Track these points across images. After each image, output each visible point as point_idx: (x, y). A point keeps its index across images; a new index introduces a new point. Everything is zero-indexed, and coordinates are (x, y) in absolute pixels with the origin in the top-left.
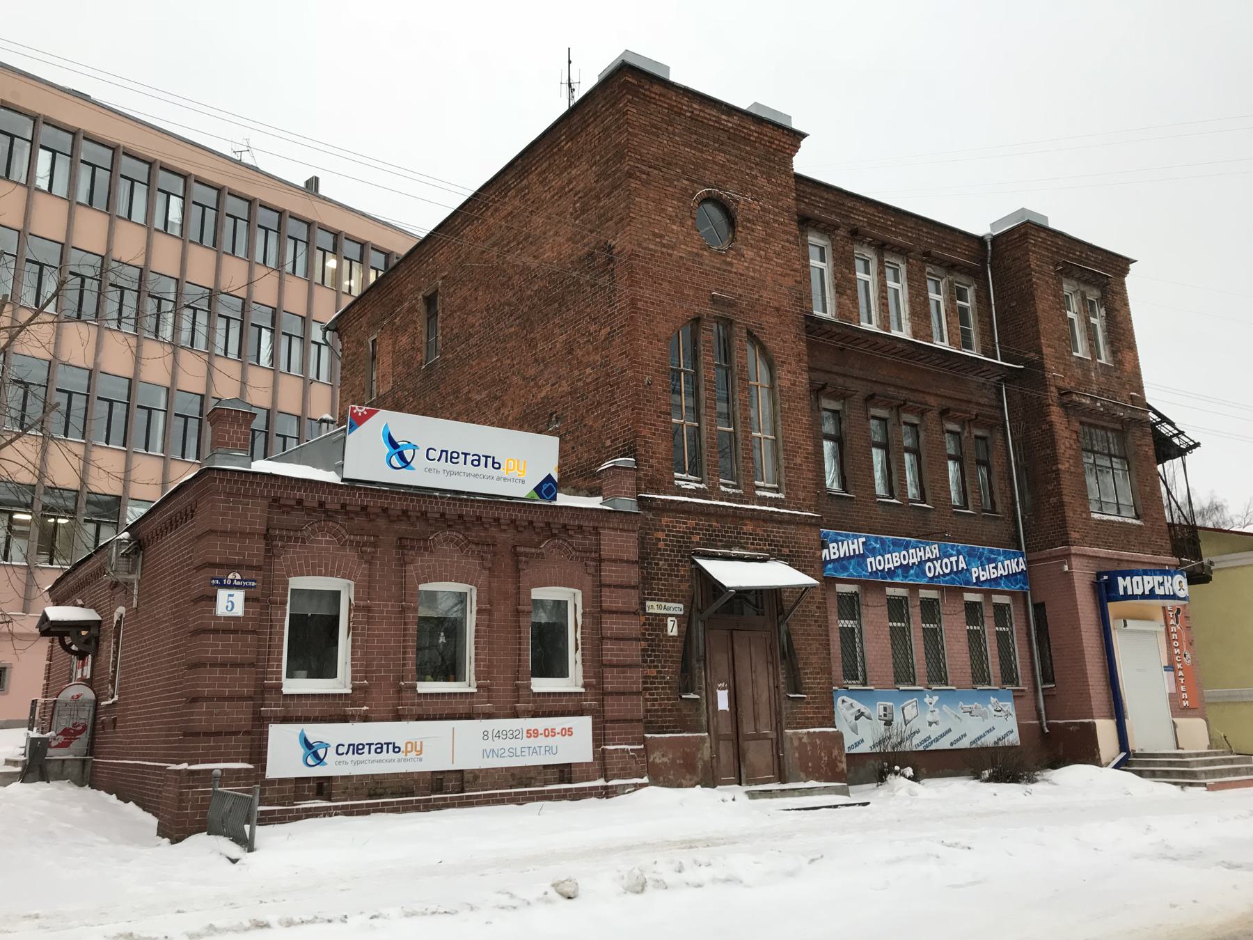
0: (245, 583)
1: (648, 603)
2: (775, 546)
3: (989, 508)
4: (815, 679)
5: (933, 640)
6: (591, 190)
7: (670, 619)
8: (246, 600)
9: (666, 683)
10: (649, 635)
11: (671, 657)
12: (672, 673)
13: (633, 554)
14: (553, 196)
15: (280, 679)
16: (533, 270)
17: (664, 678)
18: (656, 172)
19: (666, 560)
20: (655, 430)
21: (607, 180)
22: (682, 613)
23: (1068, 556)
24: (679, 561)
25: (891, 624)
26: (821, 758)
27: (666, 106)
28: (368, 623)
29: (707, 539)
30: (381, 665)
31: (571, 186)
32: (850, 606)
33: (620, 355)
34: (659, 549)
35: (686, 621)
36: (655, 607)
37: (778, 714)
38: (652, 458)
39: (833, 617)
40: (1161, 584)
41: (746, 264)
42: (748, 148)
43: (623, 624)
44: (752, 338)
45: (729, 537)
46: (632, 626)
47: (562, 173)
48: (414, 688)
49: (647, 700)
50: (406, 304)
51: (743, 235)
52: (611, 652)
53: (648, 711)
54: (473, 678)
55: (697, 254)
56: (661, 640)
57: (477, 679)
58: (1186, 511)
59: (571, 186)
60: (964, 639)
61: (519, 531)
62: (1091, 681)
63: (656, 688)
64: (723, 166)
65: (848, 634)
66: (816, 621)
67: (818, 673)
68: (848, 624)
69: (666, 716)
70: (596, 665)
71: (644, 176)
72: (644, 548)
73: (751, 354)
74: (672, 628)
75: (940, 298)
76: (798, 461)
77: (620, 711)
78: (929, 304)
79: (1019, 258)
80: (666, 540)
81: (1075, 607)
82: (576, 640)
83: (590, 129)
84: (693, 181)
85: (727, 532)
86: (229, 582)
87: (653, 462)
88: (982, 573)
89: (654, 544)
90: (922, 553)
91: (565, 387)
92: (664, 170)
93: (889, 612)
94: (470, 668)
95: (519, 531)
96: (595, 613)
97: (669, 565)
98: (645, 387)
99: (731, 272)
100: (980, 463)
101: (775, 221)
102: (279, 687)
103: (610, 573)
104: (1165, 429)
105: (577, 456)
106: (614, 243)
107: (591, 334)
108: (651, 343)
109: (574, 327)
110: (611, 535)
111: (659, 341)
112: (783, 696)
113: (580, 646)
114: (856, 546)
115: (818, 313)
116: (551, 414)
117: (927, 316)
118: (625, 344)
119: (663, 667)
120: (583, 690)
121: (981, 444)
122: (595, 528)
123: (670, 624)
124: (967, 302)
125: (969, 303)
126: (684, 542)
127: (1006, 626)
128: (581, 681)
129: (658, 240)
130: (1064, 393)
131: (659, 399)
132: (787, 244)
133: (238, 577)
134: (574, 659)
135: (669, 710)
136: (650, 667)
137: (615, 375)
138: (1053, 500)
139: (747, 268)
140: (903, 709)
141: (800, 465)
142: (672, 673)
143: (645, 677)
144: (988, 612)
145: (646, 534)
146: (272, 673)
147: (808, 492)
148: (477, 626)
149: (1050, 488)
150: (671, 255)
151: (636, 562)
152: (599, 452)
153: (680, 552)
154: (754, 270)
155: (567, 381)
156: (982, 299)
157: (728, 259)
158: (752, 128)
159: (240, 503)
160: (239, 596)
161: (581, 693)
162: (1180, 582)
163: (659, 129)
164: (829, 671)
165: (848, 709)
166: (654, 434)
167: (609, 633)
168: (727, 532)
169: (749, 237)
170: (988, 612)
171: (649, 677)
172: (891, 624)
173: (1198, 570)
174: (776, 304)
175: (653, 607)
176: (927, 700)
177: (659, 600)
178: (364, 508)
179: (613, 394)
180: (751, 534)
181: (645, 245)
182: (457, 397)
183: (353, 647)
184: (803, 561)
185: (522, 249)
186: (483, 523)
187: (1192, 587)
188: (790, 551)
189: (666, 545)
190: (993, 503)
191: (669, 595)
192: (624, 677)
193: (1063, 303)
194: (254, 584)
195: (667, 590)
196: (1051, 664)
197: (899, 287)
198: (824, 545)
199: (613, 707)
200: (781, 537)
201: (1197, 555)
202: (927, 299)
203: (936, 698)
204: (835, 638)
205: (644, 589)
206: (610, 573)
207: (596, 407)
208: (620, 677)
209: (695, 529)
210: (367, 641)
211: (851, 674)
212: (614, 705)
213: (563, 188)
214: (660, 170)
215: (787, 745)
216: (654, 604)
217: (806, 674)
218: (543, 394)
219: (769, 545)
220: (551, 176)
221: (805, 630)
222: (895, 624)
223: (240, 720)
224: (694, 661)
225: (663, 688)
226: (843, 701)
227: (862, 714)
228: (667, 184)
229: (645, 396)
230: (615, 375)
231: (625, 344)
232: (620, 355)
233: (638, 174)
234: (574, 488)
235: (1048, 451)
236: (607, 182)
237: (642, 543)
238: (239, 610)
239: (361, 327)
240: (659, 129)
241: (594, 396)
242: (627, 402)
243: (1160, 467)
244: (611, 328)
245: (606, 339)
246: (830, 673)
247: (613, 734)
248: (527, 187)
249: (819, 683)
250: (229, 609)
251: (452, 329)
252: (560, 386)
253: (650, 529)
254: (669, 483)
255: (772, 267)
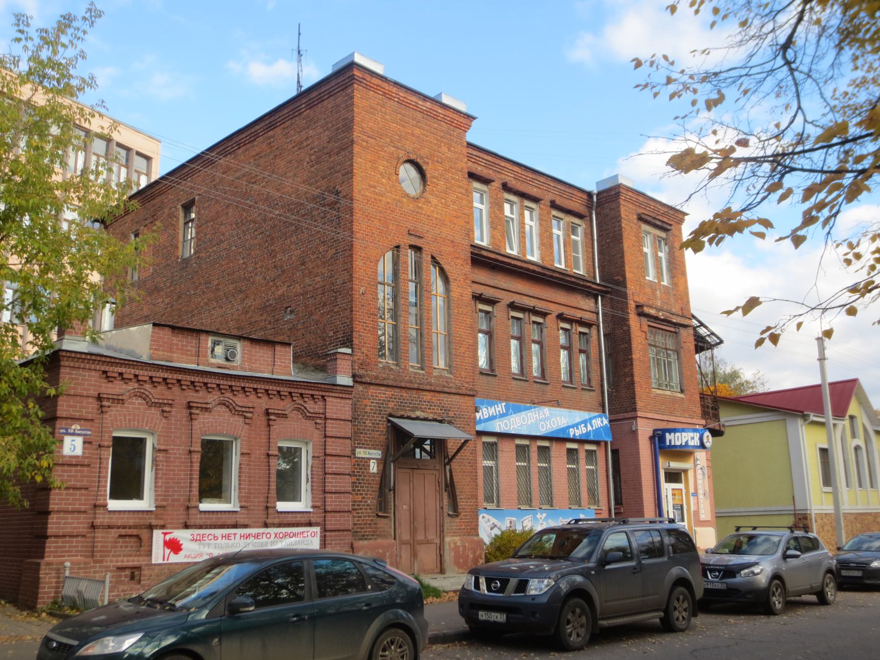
0: (83, 432)
1: (358, 450)
2: (445, 410)
3: (586, 383)
4: (467, 502)
5: (546, 474)
6: (323, 148)
7: (372, 461)
8: (84, 442)
9: (368, 505)
10: (357, 472)
11: (372, 487)
12: (372, 498)
13: (348, 415)
14: (294, 147)
15: (105, 500)
16: (276, 199)
17: (366, 502)
18: (372, 140)
19: (370, 420)
20: (366, 326)
21: (337, 142)
22: (380, 457)
23: (635, 418)
24: (379, 421)
25: (517, 464)
26: (468, 556)
27: (381, 93)
28: (166, 461)
29: (399, 406)
30: (175, 491)
31: (308, 142)
32: (491, 450)
33: (342, 271)
34: (366, 412)
35: (384, 463)
36: (362, 453)
37: (442, 526)
38: (363, 346)
39: (480, 458)
40: (693, 438)
41: (432, 209)
42: (436, 125)
43: (340, 464)
44: (435, 261)
45: (415, 404)
46: (345, 465)
47: (301, 131)
48: (197, 507)
49: (354, 517)
50: (167, 211)
51: (430, 187)
52: (332, 483)
53: (355, 524)
54: (237, 500)
55: (399, 201)
56: (365, 476)
57: (240, 501)
58: (712, 388)
59: (308, 142)
60: (564, 473)
61: (258, 397)
62: (646, 504)
63: (361, 509)
64: (418, 137)
65: (488, 470)
66: (469, 463)
67: (469, 499)
68: (489, 463)
69: (366, 528)
70: (322, 492)
71: (364, 144)
72: (356, 412)
73: (434, 272)
74: (373, 468)
75: (560, 233)
76: (462, 350)
77: (336, 524)
78: (552, 238)
79: (614, 209)
80: (371, 406)
81: (638, 453)
82: (307, 475)
83: (325, 103)
84: (397, 148)
85: (412, 400)
86: (72, 431)
87: (364, 350)
88: (576, 431)
89: (363, 409)
90: (537, 415)
91: (298, 289)
92: (378, 139)
93: (517, 456)
94: (234, 494)
95: (258, 397)
96: (323, 456)
97: (373, 424)
98: (360, 295)
99: (421, 214)
100: (581, 351)
101: (453, 178)
102: (105, 506)
103: (332, 428)
104: (702, 331)
105: (306, 341)
106: (341, 189)
107: (321, 253)
108: (365, 264)
109: (307, 246)
110: (333, 402)
111: (371, 262)
112: (446, 514)
113: (310, 480)
114: (500, 409)
115: (477, 242)
116: (287, 308)
117: (551, 246)
118: (346, 263)
119: (366, 494)
120: (311, 510)
121: (583, 338)
122: (323, 396)
123: (372, 465)
124: (578, 236)
125: (578, 238)
126: (384, 407)
127: (593, 465)
128: (310, 504)
129: (372, 189)
130: (639, 306)
131: (369, 304)
132: (460, 195)
133: (78, 427)
134: (305, 487)
135: (370, 524)
136: (357, 494)
137: (338, 285)
138: (628, 379)
139: (433, 211)
140: (522, 522)
141: (464, 353)
142: (372, 498)
143: (354, 501)
144: (582, 455)
145: (358, 401)
146: (101, 495)
147: (469, 372)
148: (240, 464)
149: (626, 371)
150: (380, 201)
151: (351, 421)
152: (324, 340)
153: (380, 414)
154: (437, 213)
155: (300, 285)
156: (589, 234)
157: (420, 205)
158: (439, 111)
159: (80, 375)
160: (79, 441)
161: (310, 512)
162: (708, 436)
163: (376, 109)
164: (475, 497)
165: (486, 523)
166: (365, 330)
167: (330, 471)
168: (412, 400)
169: (435, 189)
170: (582, 455)
171: (356, 501)
172: (517, 464)
173: (717, 428)
174: (452, 238)
175: (361, 453)
176: (539, 516)
177: (365, 448)
178: (165, 379)
179: (336, 299)
180: (429, 402)
181: (363, 192)
182: (208, 288)
183: (156, 478)
184: (463, 421)
185: (267, 182)
186: (245, 392)
187: (716, 438)
188: (455, 414)
189: (371, 409)
190: (589, 380)
191: (372, 445)
192: (340, 502)
193: (640, 243)
194: (89, 433)
195: (371, 441)
196: (621, 491)
197: (531, 222)
198: (477, 410)
199: (333, 521)
200: (449, 404)
201: (716, 417)
202: (551, 234)
203: (544, 515)
204: (480, 473)
205: (355, 440)
206: (332, 428)
207: (323, 306)
208: (336, 501)
209: (391, 398)
210: (165, 474)
211: (489, 499)
212: (332, 521)
213: (302, 142)
214: (375, 139)
215: (447, 547)
216: (362, 450)
217: (461, 499)
218: (280, 292)
219: (441, 410)
220: (292, 132)
221: (462, 469)
222: (520, 464)
223: (79, 528)
224: (387, 490)
225: (365, 509)
226: (483, 517)
227: (495, 526)
228: (380, 149)
229: (360, 302)
230: (338, 285)
231: (346, 263)
232: (342, 271)
233: (360, 141)
234: (303, 364)
235: (626, 346)
236: (336, 145)
237: (354, 408)
238: (79, 452)
239: (125, 223)
240: (376, 109)
241: (321, 298)
242: (347, 305)
243: (697, 356)
244: (336, 250)
245: (332, 258)
246: (477, 499)
247: (331, 540)
248: (273, 137)
249: (469, 506)
250: (72, 449)
251: (206, 235)
252: (294, 288)
253: (360, 398)
254: (374, 365)
255: (449, 211)
